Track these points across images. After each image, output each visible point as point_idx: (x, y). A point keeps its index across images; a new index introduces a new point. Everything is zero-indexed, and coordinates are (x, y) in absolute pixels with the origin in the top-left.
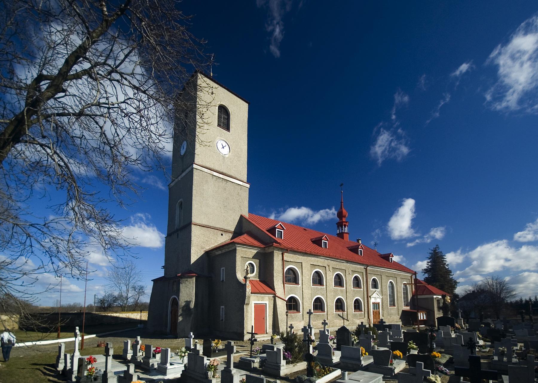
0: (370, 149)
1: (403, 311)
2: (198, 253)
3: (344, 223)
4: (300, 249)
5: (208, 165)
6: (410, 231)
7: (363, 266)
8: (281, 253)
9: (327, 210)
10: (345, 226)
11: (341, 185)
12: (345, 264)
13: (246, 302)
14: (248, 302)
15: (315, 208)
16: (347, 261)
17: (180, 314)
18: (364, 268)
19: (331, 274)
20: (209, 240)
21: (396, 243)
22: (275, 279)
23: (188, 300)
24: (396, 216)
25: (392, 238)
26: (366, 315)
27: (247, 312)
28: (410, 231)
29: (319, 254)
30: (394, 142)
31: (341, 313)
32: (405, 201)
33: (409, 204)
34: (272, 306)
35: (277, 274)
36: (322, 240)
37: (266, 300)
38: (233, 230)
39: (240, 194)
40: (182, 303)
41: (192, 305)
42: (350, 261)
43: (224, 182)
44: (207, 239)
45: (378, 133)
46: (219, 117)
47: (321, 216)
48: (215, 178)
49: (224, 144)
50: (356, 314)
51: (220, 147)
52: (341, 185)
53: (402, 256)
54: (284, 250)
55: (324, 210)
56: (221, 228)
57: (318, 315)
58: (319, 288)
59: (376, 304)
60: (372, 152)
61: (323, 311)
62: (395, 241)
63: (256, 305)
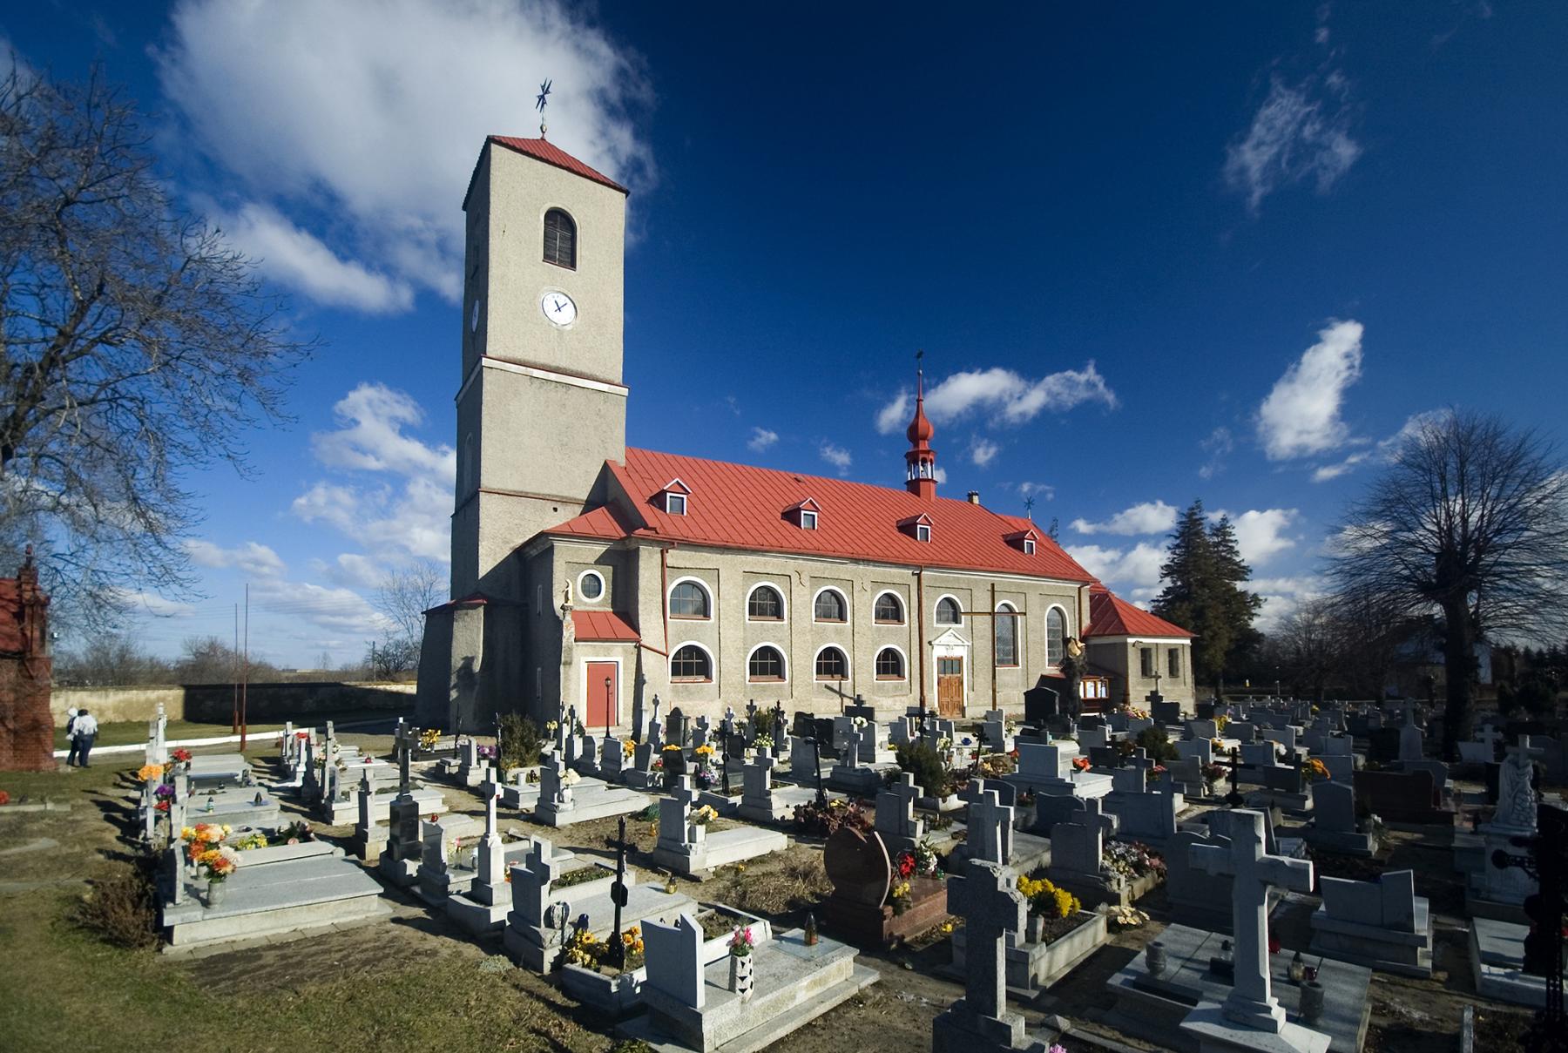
0: (1223, 158)
1: (1042, 676)
2: (495, 554)
3: (921, 456)
4: (738, 540)
5: (519, 355)
6: (1337, 429)
7: (909, 569)
8: (659, 549)
9: (1070, 373)
10: (924, 461)
11: (919, 355)
12: (851, 567)
13: (563, 659)
14: (568, 660)
15: (1031, 372)
16: (856, 561)
17: (452, 684)
18: (913, 574)
19: (806, 591)
20: (523, 523)
21: (1280, 470)
22: (641, 607)
23: (470, 655)
24: (1291, 381)
25: (1269, 457)
26: (916, 687)
27: (567, 679)
28: (1337, 429)
29: (767, 548)
30: (1313, 124)
31: (835, 684)
32: (1332, 328)
33: (1346, 336)
34: (634, 667)
35: (649, 597)
36: (799, 510)
37: (619, 655)
38: (584, 496)
39: (602, 412)
40: (457, 662)
41: (477, 667)
42: (863, 560)
43: (563, 390)
44: (517, 522)
45: (1263, 96)
46: (548, 237)
47: (1049, 393)
48: (538, 382)
49: (562, 300)
50: (884, 685)
51: (550, 307)
52: (919, 355)
53: (1294, 511)
54: (666, 544)
55: (1058, 375)
56: (553, 496)
57: (764, 687)
58: (768, 625)
59: (952, 660)
60: (1231, 166)
61: (781, 676)
62: (1281, 463)
63: (592, 667)
